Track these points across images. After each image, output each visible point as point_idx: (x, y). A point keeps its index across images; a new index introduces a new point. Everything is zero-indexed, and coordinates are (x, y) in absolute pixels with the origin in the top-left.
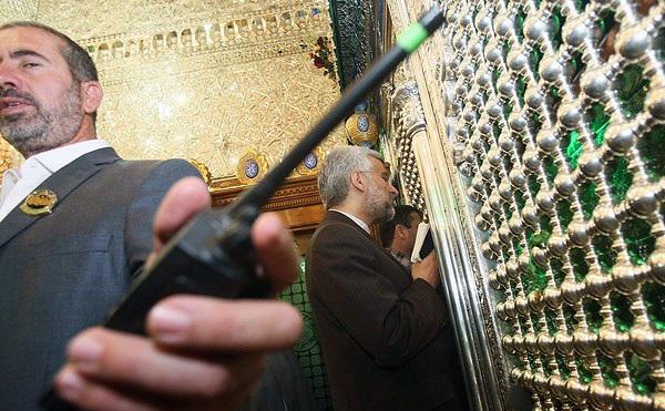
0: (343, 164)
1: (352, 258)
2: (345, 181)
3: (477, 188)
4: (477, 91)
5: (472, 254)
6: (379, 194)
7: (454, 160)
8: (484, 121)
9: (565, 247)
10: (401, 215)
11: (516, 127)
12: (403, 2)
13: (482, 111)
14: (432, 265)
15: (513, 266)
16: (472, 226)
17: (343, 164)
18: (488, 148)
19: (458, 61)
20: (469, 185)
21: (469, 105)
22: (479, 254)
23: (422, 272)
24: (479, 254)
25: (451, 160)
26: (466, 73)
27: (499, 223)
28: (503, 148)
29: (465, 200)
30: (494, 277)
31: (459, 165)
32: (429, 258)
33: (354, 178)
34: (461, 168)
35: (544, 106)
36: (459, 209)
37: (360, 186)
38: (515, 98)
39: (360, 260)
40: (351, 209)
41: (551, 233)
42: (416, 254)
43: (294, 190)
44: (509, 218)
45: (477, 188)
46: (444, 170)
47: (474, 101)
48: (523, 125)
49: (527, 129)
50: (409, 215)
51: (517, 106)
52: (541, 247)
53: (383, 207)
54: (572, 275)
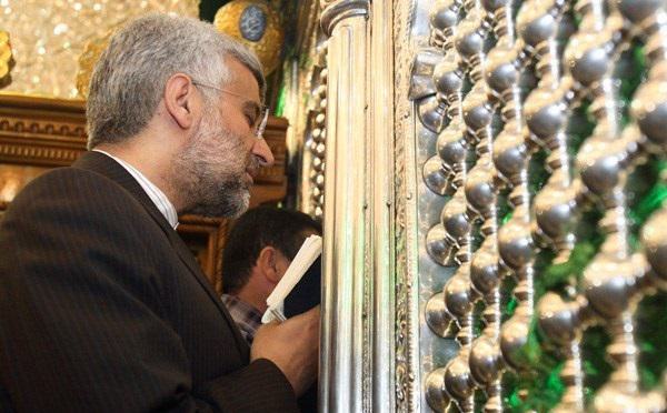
0: (159, 52)
1: (98, 257)
2: (152, 90)
3: (452, 302)
4: (477, 23)
5: (401, 318)
6: (222, 149)
7: (413, 85)
8: (513, 140)
9: (629, 291)
10: (267, 212)
11: (584, 74)
12: (358, 409)
13: (484, 150)
14: (299, 343)
15: (487, 350)
16: (416, 251)
17: (159, 52)
18: (505, 211)
19: (452, 15)
20: (438, 290)
21: (459, 123)
22: (417, 321)
23: (275, 344)
24: (417, 321)
25: (403, 88)
26: (465, 49)
27: (481, 326)
28: (541, 224)
29: (415, 187)
30: (438, 381)
31: (419, 100)
32: (302, 321)
33: (174, 88)
34: (423, 108)
35: (608, 84)
36: (395, 208)
37: (181, 113)
38: (607, 102)
39: (119, 269)
40: (147, 162)
41: (597, 249)
42: (276, 299)
43: (57, 126)
44: (505, 318)
45: (452, 302)
46: (382, 109)
47: (497, 82)
48: (557, 125)
49: (561, 136)
50: (285, 222)
51: (609, 123)
52: (565, 297)
53: (222, 181)
54: (630, 372)
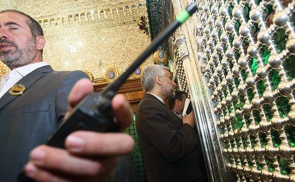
0: (152, 73)
1: (156, 114)
2: (153, 80)
3: (212, 83)
4: (212, 40)
5: (209, 112)
6: (168, 86)
7: (202, 71)
8: (215, 53)
9: (250, 110)
10: (178, 95)
11: (229, 56)
12: (179, 1)
13: (214, 49)
14: (192, 117)
15: (228, 118)
16: (209, 100)
17: (152, 73)
18: (217, 65)
19: (203, 27)
20: (208, 82)
21: (208, 47)
22: (212, 113)
23: (187, 120)
24: (212, 113)
25: (200, 71)
26: (207, 33)
27: (221, 99)
28: (223, 65)
29: (206, 89)
30: (219, 123)
31: (204, 73)
32: (191, 114)
33: (157, 79)
34: (205, 74)
35: (241, 47)
36: (204, 93)
37: (160, 82)
38: (228, 43)
39: (160, 115)
40: (156, 93)
41: (244, 103)
42: (184, 112)
43: (130, 84)
44: (226, 97)
45: (212, 83)
46: (197, 75)
47: (210, 45)
48: (232, 55)
49: (234, 57)
50: (181, 95)
51: (229, 47)
52: (240, 109)
53: (170, 92)
54: (254, 122)
